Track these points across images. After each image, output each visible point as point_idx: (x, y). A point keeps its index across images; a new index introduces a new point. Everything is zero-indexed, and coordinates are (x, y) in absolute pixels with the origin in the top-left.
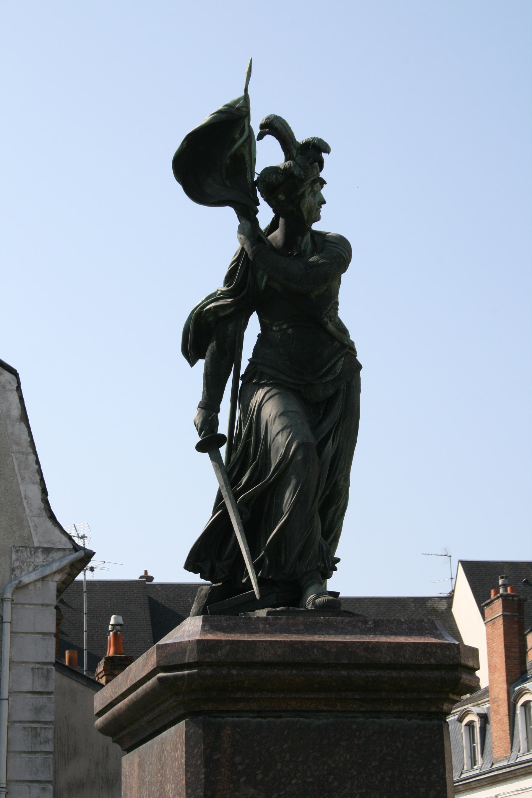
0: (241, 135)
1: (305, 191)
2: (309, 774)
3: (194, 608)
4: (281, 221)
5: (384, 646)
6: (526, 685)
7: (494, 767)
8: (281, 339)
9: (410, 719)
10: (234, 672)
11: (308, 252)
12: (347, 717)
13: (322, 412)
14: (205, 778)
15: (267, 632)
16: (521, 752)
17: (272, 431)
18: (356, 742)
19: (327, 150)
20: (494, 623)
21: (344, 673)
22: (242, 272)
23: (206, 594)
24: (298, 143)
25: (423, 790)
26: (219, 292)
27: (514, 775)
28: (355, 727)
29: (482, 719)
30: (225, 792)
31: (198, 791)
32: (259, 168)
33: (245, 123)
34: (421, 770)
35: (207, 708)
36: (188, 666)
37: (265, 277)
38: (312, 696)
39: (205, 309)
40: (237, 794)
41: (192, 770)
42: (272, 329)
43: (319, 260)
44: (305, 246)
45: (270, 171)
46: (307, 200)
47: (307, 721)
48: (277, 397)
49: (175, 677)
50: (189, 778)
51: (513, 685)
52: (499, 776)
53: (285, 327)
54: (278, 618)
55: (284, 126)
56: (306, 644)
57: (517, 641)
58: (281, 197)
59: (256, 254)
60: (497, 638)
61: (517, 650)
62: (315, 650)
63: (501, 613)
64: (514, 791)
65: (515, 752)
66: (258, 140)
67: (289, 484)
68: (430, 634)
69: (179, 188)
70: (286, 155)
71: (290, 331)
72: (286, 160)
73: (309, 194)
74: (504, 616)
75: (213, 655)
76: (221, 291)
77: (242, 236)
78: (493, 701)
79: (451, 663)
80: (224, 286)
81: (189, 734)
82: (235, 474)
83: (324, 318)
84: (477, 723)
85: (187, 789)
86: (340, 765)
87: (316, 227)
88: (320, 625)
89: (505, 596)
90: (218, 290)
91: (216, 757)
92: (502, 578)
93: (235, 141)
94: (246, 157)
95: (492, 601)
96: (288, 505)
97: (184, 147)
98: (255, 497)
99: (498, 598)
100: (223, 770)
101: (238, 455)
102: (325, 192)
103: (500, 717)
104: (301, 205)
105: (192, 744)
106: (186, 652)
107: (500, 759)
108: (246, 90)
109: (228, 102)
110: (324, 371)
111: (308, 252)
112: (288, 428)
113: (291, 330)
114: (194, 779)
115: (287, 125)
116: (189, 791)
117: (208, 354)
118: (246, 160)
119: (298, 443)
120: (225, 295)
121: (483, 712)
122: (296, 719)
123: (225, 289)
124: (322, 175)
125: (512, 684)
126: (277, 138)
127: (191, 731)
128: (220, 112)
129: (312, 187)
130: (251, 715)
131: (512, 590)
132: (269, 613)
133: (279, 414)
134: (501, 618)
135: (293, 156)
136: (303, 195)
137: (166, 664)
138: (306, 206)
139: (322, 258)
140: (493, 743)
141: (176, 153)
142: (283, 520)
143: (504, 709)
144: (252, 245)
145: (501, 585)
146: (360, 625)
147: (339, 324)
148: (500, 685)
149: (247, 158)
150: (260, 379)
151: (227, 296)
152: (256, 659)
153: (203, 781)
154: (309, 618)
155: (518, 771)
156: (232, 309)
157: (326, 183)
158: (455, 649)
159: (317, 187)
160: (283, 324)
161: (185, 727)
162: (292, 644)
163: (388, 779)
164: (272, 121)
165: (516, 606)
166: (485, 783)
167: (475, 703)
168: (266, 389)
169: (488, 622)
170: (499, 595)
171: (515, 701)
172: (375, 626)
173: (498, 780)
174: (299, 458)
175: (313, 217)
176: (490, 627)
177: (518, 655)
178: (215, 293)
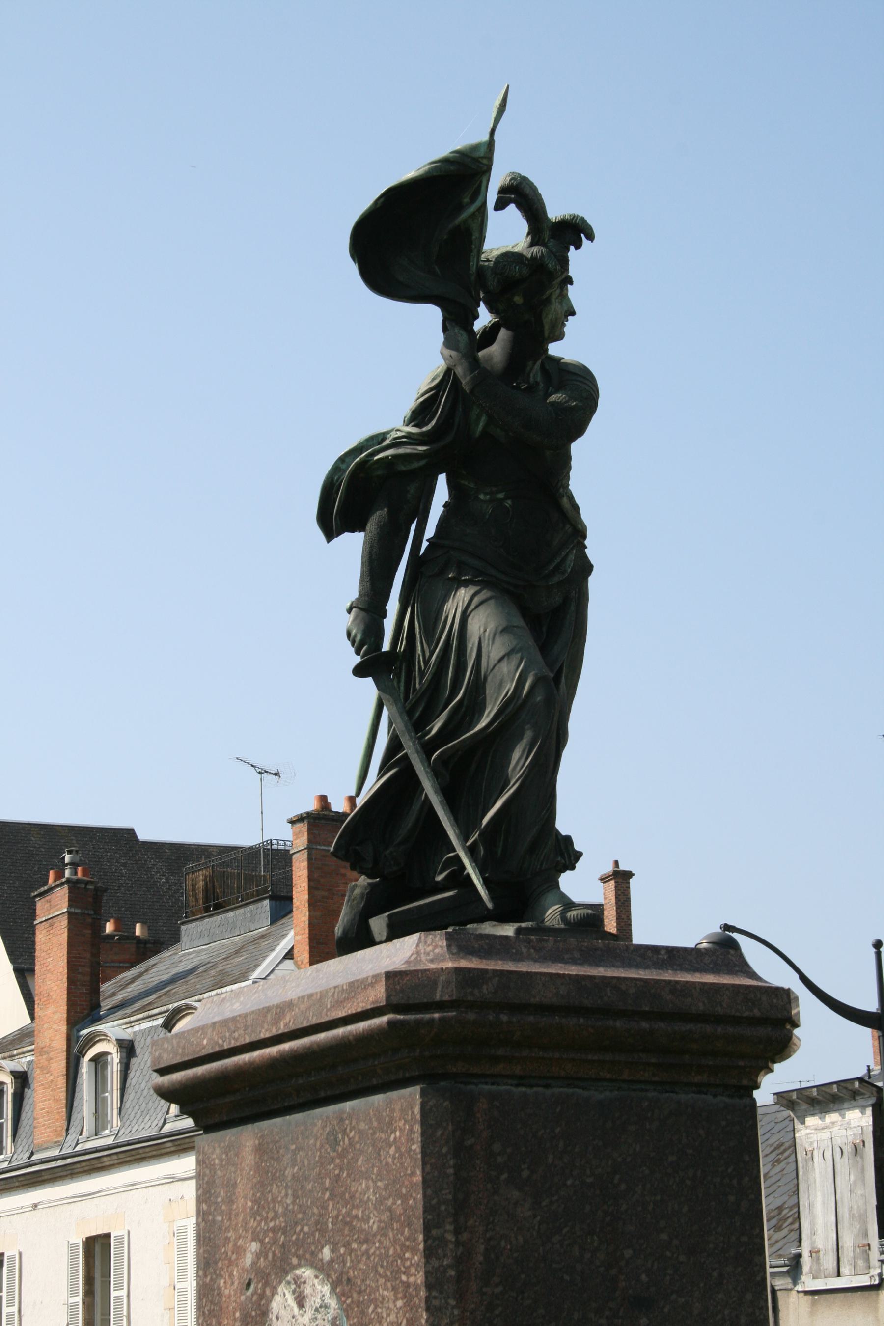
0: (473, 200)
2: (588, 1172)
5: (695, 988)
6: (101, 1027)
7: (33, 1158)
8: (475, 516)
9: (715, 1096)
10: (504, 1018)
12: (634, 1090)
13: (544, 629)
14: (455, 1174)
15: (535, 961)
16: (85, 1134)
17: (491, 655)
18: (648, 1126)
20: (51, 925)
21: (645, 1025)
23: (362, 895)
25: (732, 1198)
27: (69, 1172)
28: (646, 1104)
29: (19, 1081)
30: (480, 1196)
31: (444, 1192)
33: (481, 182)
34: (730, 1170)
35: (455, 1070)
36: (440, 1006)
38: (596, 1058)
39: (376, 458)
40: (496, 1198)
41: (433, 1161)
42: (477, 498)
45: (509, 258)
46: (553, 307)
47: (586, 1093)
48: (492, 602)
49: (418, 1022)
50: (428, 1173)
51: (77, 1027)
52: (43, 1173)
53: (501, 496)
54: (543, 940)
56: (597, 981)
57: (88, 955)
58: (518, 299)
60: (55, 949)
61: (88, 970)
62: (608, 989)
63: (66, 910)
64: (67, 1198)
65: (74, 1136)
67: (521, 738)
68: (741, 972)
69: (353, 269)
71: (508, 503)
72: (532, 245)
74: (69, 913)
75: (476, 992)
78: (42, 1051)
79: (780, 1016)
81: (428, 1107)
82: (418, 714)
84: (10, 1086)
85: (425, 1188)
86: (629, 1160)
87: (554, 349)
88: (599, 952)
89: (74, 882)
91: (468, 1143)
92: (70, 852)
93: (461, 208)
95: (51, 889)
96: (518, 768)
98: (460, 753)
99: (62, 884)
100: (478, 1162)
101: (425, 686)
102: (572, 292)
103: (51, 1078)
104: (544, 315)
105: (432, 1122)
106: (436, 984)
107: (45, 1146)
110: (551, 567)
112: (517, 652)
113: (509, 502)
114: (436, 1174)
116: (429, 1192)
117: (371, 525)
118: (474, 237)
119: (536, 675)
121: (21, 1069)
122: (571, 1091)
125: (75, 1025)
127: (431, 1103)
128: (445, 161)
130: (509, 1082)
131: (85, 873)
132: (518, 931)
133: (500, 628)
134: (66, 917)
135: (544, 240)
136: (548, 301)
137: (403, 1002)
138: (550, 316)
139: (572, 398)
140: (35, 1119)
141: (362, 215)
142: (512, 791)
143: (59, 1065)
145: (68, 864)
148: (55, 1027)
149: (475, 235)
150: (460, 574)
152: (533, 1000)
153: (452, 1178)
155: (78, 1166)
158: (785, 996)
161: (421, 1096)
162: (577, 979)
163: (688, 1182)
164: (520, 183)
165: (91, 900)
166: (17, 1184)
167: (7, 1054)
168: (472, 590)
169: (41, 922)
170: (64, 880)
171: (81, 1053)
172: (669, 957)
173: (40, 1179)
174: (539, 699)
176: (45, 931)
177: (87, 978)
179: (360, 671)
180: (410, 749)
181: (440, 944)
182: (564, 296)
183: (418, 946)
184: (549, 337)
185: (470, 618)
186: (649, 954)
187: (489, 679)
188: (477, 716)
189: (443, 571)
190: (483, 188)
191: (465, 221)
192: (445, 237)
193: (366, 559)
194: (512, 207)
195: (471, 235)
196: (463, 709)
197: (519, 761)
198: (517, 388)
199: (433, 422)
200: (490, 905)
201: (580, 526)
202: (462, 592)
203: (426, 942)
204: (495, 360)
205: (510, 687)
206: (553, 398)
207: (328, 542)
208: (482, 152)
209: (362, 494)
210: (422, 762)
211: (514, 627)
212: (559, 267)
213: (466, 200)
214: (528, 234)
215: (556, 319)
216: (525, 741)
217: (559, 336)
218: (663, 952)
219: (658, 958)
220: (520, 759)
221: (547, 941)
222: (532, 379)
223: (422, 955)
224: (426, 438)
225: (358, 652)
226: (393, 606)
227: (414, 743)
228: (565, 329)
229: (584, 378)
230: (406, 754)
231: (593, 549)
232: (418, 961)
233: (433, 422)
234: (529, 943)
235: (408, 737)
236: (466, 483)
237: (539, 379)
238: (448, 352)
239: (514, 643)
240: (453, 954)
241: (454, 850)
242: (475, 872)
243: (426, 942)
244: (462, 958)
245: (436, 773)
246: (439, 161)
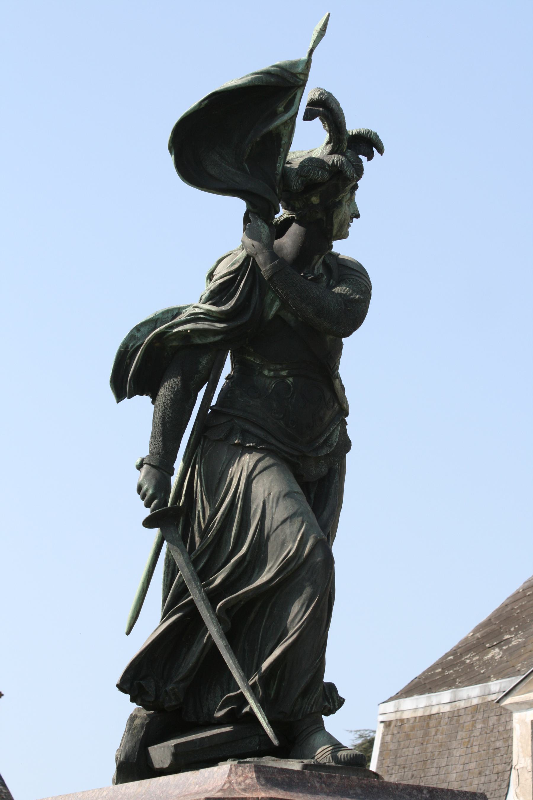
0: (287, 109)
3: (306, 761)
17: (275, 516)
22: (246, 291)
23: (142, 725)
33: (296, 94)
39: (175, 330)
42: (261, 374)
48: (274, 468)
53: (284, 373)
54: (332, 776)
58: (315, 200)
66: (306, 118)
69: (170, 160)
72: (331, 153)
73: (346, 202)
82: (201, 565)
87: (339, 247)
88: (376, 790)
93: (275, 115)
94: (280, 140)
96: (297, 620)
97: (202, 107)
98: (242, 603)
104: (335, 216)
112: (298, 516)
113: (291, 379)
117: (165, 391)
118: (283, 142)
119: (316, 538)
128: (267, 73)
132: (305, 767)
133: (283, 493)
136: (340, 203)
138: (340, 217)
142: (290, 640)
146: (416, 794)
149: (284, 140)
150: (244, 441)
151: (212, 319)
154: (364, 779)
160: (282, 369)
164: (327, 99)
168: (256, 456)
174: (318, 559)
179: (149, 523)
180: (196, 595)
181: (250, 775)
183: (229, 776)
184: (336, 235)
185: (254, 481)
186: (415, 792)
187: (272, 538)
188: (257, 570)
189: (228, 437)
190: (297, 100)
191: (277, 128)
192: (258, 139)
193: (159, 420)
194: (317, 120)
195: (281, 139)
196: (246, 563)
197: (297, 615)
199: (232, 302)
200: (276, 742)
201: (345, 406)
202: (247, 457)
203: (236, 774)
205: (292, 547)
206: (338, 290)
207: (118, 402)
208: (300, 69)
209: (150, 362)
210: (207, 608)
211: (295, 492)
212: (355, 175)
213: (281, 109)
214: (328, 143)
215: (345, 220)
216: (304, 596)
217: (343, 235)
218: (425, 792)
219: (422, 797)
220: (298, 612)
221: (335, 777)
222: (316, 271)
223: (235, 785)
224: (223, 317)
225: (148, 505)
226: (179, 465)
227: (200, 590)
228: (350, 230)
230: (192, 601)
231: (354, 426)
232: (231, 789)
233: (232, 302)
234: (321, 779)
235: (194, 586)
236: (252, 359)
237: (321, 271)
238: (249, 242)
239: (296, 507)
240: (262, 785)
241: (239, 688)
242: (260, 711)
243: (236, 774)
244: (270, 789)
245: (220, 620)
246: (262, 73)
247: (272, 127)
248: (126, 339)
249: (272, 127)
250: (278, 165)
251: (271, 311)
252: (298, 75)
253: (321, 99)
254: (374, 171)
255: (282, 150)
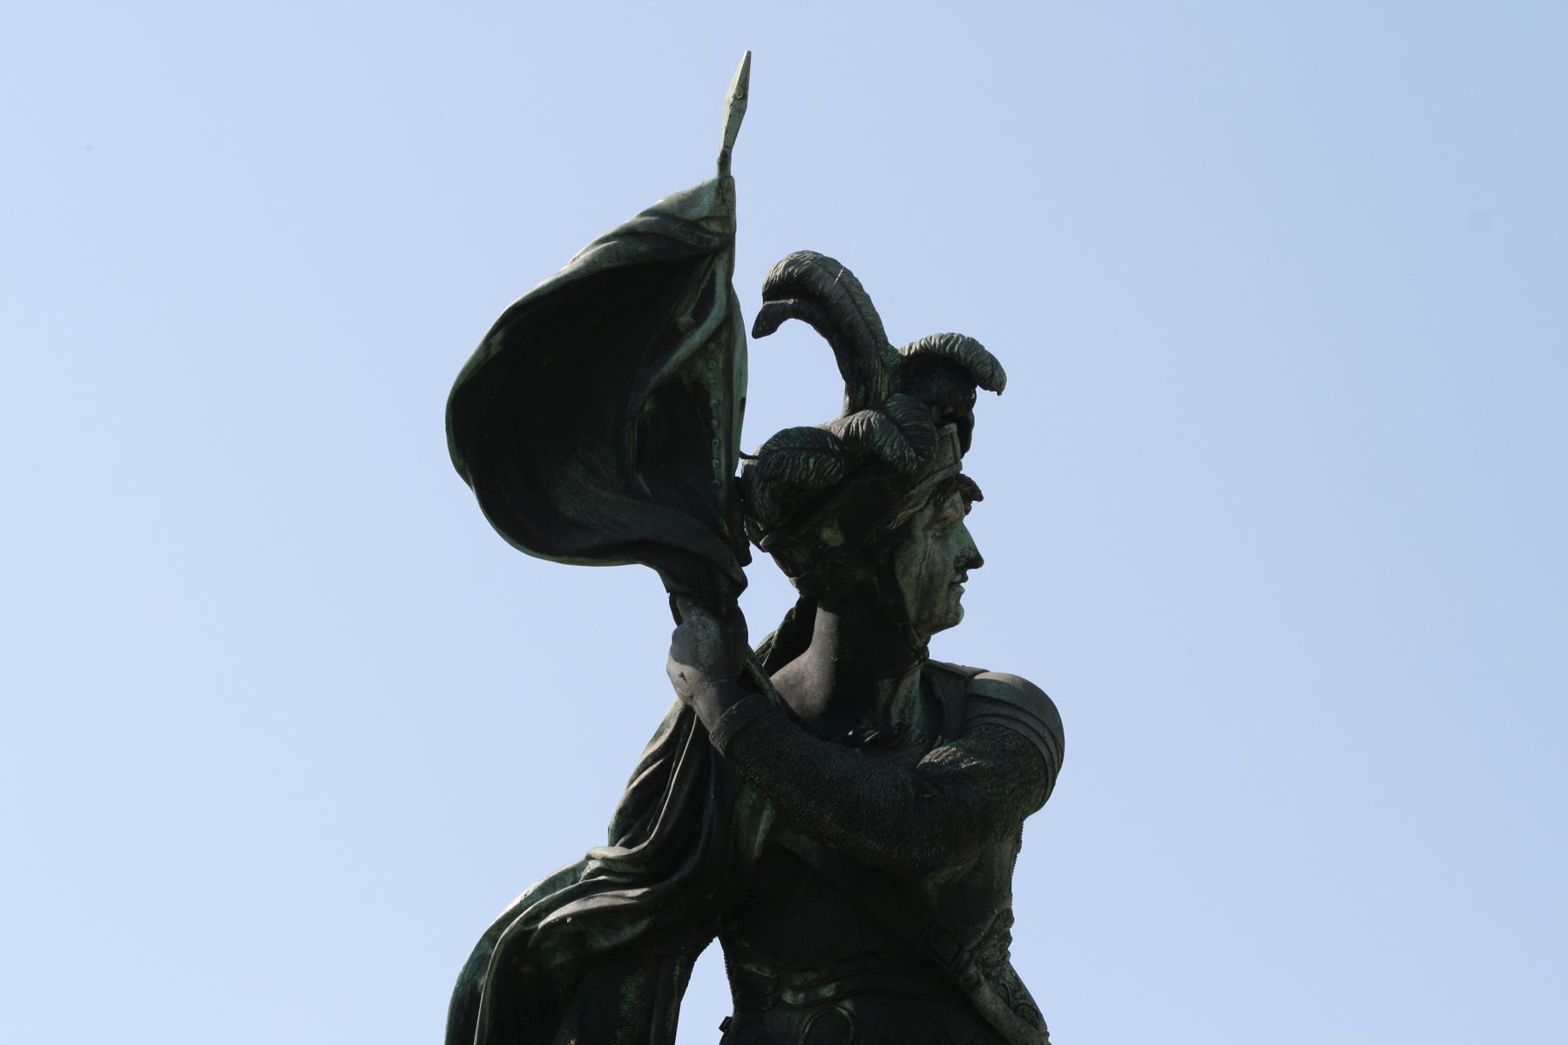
0: (700, 314)
1: (911, 519)
4: (823, 621)
11: (916, 731)
19: (994, 379)
24: (894, 351)
26: (593, 865)
32: (753, 437)
33: (714, 274)
37: (767, 813)
42: (779, 1000)
43: (961, 760)
44: (902, 712)
45: (795, 444)
46: (920, 549)
53: (827, 991)
55: (848, 291)
58: (831, 536)
59: (737, 731)
66: (757, 333)
70: (851, 390)
72: (853, 409)
73: (926, 529)
76: (605, 859)
77: (688, 670)
80: (612, 844)
83: (967, 964)
87: (944, 648)
90: (589, 858)
93: (676, 336)
94: (714, 392)
97: (494, 351)
102: (978, 523)
104: (899, 569)
108: (725, 160)
109: (658, 200)
111: (916, 731)
113: (848, 1004)
115: (860, 287)
118: (713, 402)
120: (613, 874)
123: (618, 852)
124: (970, 466)
126: (824, 333)
128: (628, 234)
129: (939, 508)
136: (906, 531)
138: (914, 570)
139: (970, 753)
141: (462, 373)
144: (724, 700)
147: (1015, 992)
149: (717, 396)
151: (624, 880)
156: (642, 925)
157: (980, 498)
159: (953, 505)
160: (822, 983)
164: (810, 271)
175: (937, 611)
178: (574, 871)
182: (950, 529)
195: (708, 397)
198: (857, 741)
204: (808, 684)
208: (704, 208)
213: (685, 319)
217: (951, 617)
224: (643, 870)
228: (964, 601)
229: (1020, 709)
238: (678, 668)
246: (615, 236)
247: (668, 367)
248: (466, 967)
249: (668, 367)
250: (715, 462)
251: (756, 833)
252: (703, 224)
253: (790, 274)
254: (999, 442)
255: (715, 422)
